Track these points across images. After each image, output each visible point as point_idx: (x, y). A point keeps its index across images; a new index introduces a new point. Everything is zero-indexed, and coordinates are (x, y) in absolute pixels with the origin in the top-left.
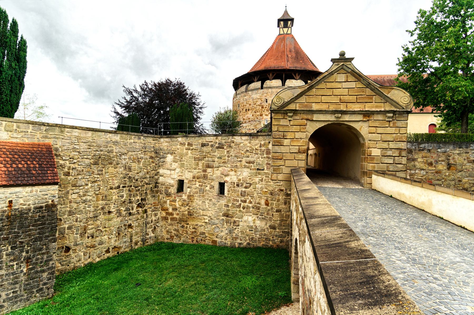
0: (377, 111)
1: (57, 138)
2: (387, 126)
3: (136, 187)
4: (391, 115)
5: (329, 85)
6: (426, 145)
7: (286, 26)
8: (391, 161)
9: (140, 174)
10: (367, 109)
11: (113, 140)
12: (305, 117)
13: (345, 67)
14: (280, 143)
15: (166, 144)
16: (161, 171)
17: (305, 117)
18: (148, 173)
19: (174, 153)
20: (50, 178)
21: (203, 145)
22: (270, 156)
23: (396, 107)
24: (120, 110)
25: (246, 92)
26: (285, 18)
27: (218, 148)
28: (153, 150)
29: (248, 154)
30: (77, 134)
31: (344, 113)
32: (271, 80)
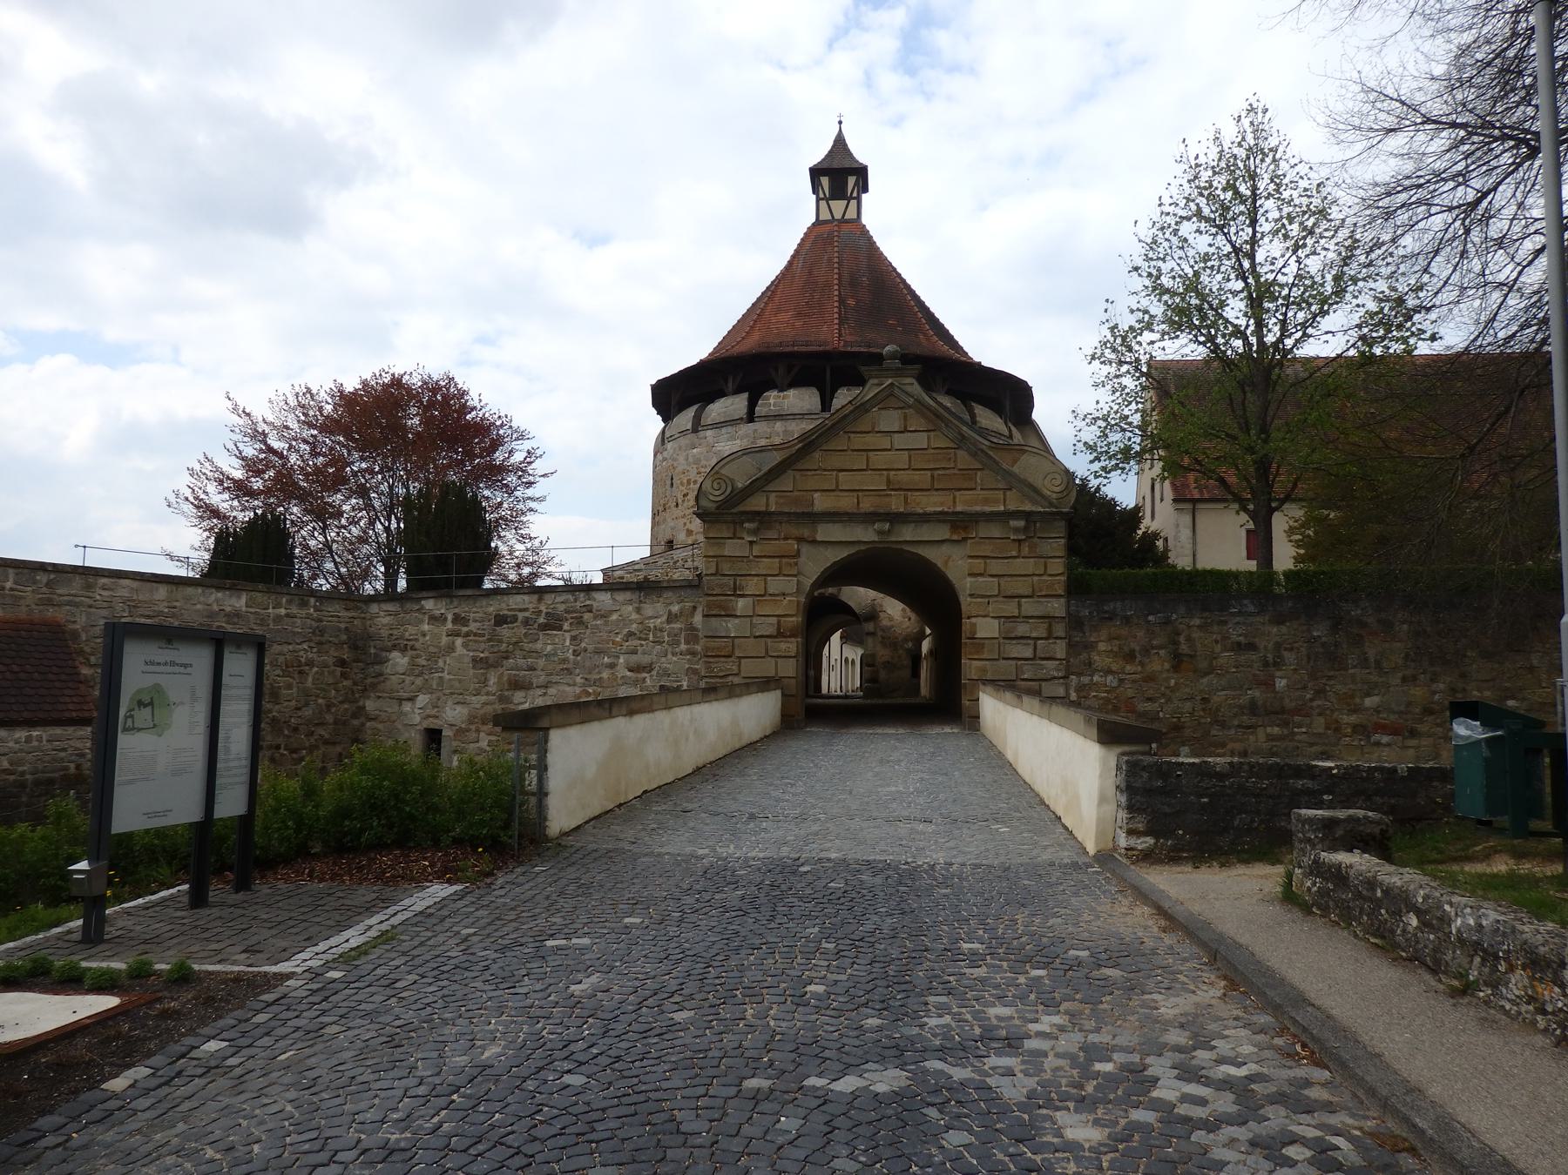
0: (984, 514)
1: (77, 605)
2: (1014, 553)
3: (294, 751)
4: (1021, 523)
5: (858, 441)
6: (1119, 604)
7: (838, 192)
8: (1028, 653)
9: (307, 712)
10: (959, 509)
11: (228, 609)
12: (795, 532)
13: (896, 391)
14: (724, 609)
15: (386, 620)
16: (370, 705)
17: (795, 532)
18: (329, 706)
19: (413, 648)
20: (71, 707)
21: (501, 620)
22: (698, 648)
23: (1034, 502)
24: (220, 500)
25: (695, 430)
26: (835, 166)
27: (545, 627)
28: (344, 637)
29: (634, 642)
30: (125, 593)
31: (896, 519)
32: (781, 390)
